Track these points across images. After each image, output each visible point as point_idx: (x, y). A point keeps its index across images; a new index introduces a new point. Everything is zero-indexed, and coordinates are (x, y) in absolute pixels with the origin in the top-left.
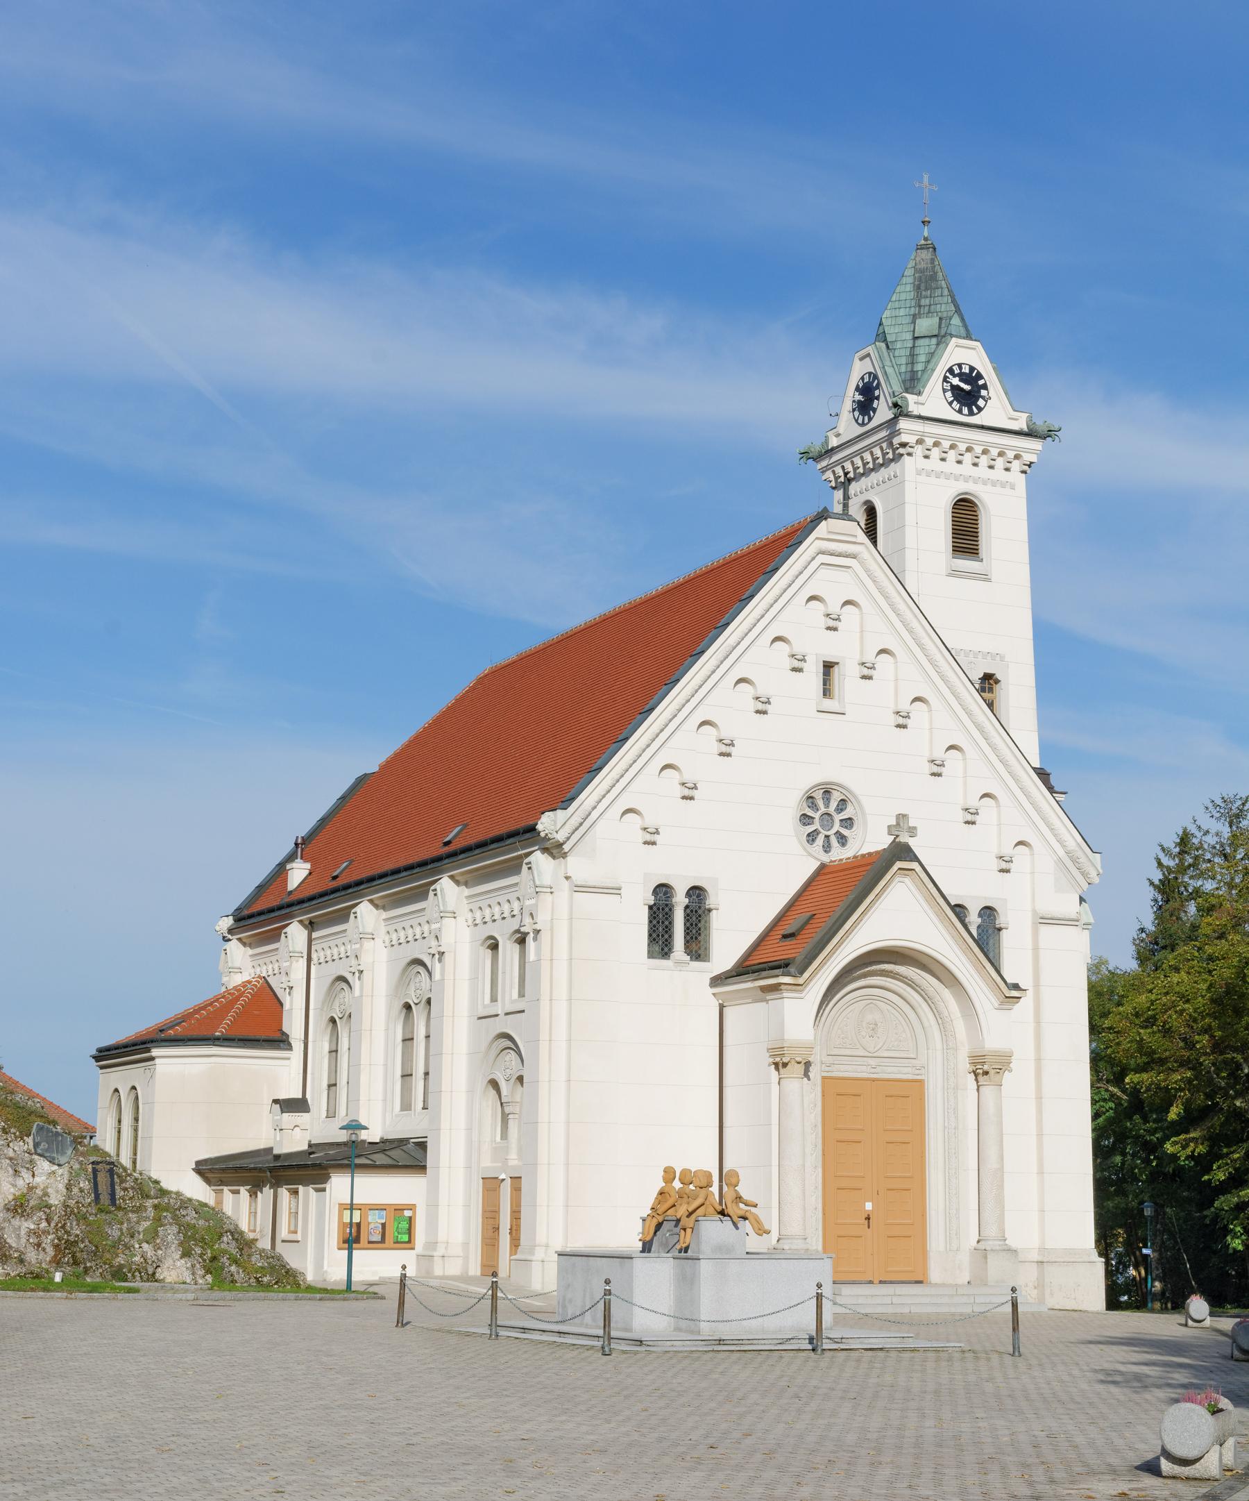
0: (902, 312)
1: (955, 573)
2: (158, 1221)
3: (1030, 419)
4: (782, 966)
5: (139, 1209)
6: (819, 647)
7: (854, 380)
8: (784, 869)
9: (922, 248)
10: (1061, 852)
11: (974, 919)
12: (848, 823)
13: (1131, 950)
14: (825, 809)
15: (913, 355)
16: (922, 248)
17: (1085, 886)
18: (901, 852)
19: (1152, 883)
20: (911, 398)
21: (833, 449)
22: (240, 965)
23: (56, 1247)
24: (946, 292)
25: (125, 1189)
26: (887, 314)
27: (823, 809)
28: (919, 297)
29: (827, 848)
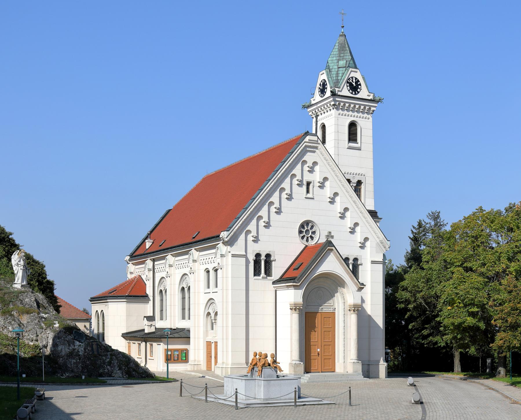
0: (335, 58)
2: (111, 359)
3: (374, 96)
5: (106, 355)
7: (319, 81)
9: (341, 36)
10: (378, 241)
11: (351, 261)
12: (314, 233)
13: (404, 259)
14: (306, 228)
15: (337, 74)
16: (341, 36)
17: (385, 251)
18: (329, 243)
20: (337, 89)
21: (313, 104)
22: (133, 271)
23: (82, 367)
24: (348, 52)
25: (101, 349)
26: (330, 59)
27: (306, 229)
28: (340, 54)
29: (307, 240)
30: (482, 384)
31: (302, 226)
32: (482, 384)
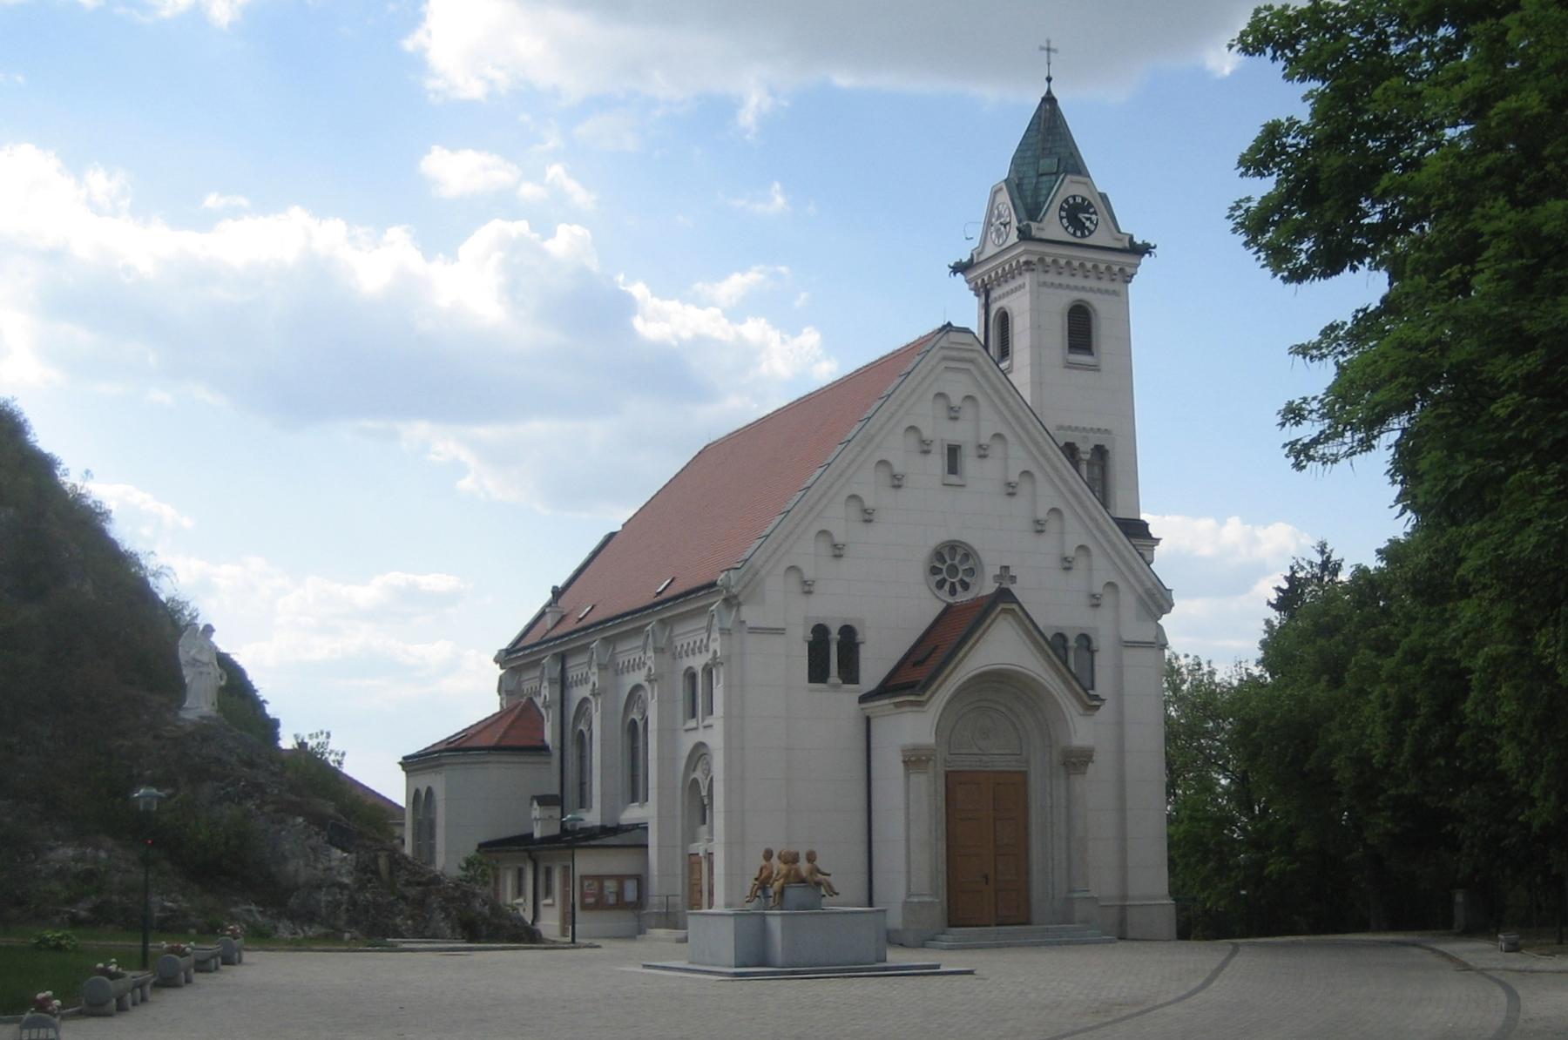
1: (1070, 366)
4: (909, 687)
6: (943, 432)
8: (919, 607)
10: (1140, 590)
14: (951, 562)
15: (1036, 189)
19: (1269, 603)
20: (1034, 225)
29: (953, 592)
30: (1443, 954)
31: (939, 555)
32: (1433, 951)
